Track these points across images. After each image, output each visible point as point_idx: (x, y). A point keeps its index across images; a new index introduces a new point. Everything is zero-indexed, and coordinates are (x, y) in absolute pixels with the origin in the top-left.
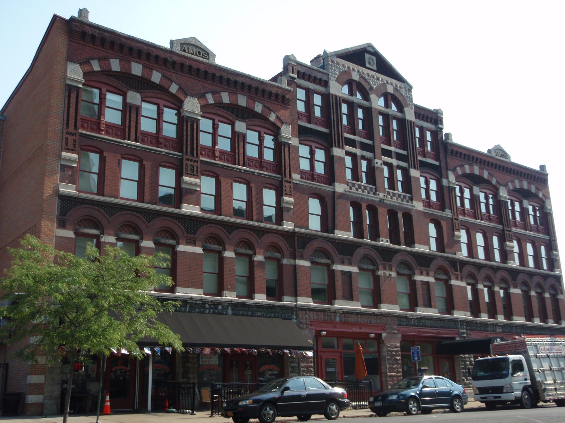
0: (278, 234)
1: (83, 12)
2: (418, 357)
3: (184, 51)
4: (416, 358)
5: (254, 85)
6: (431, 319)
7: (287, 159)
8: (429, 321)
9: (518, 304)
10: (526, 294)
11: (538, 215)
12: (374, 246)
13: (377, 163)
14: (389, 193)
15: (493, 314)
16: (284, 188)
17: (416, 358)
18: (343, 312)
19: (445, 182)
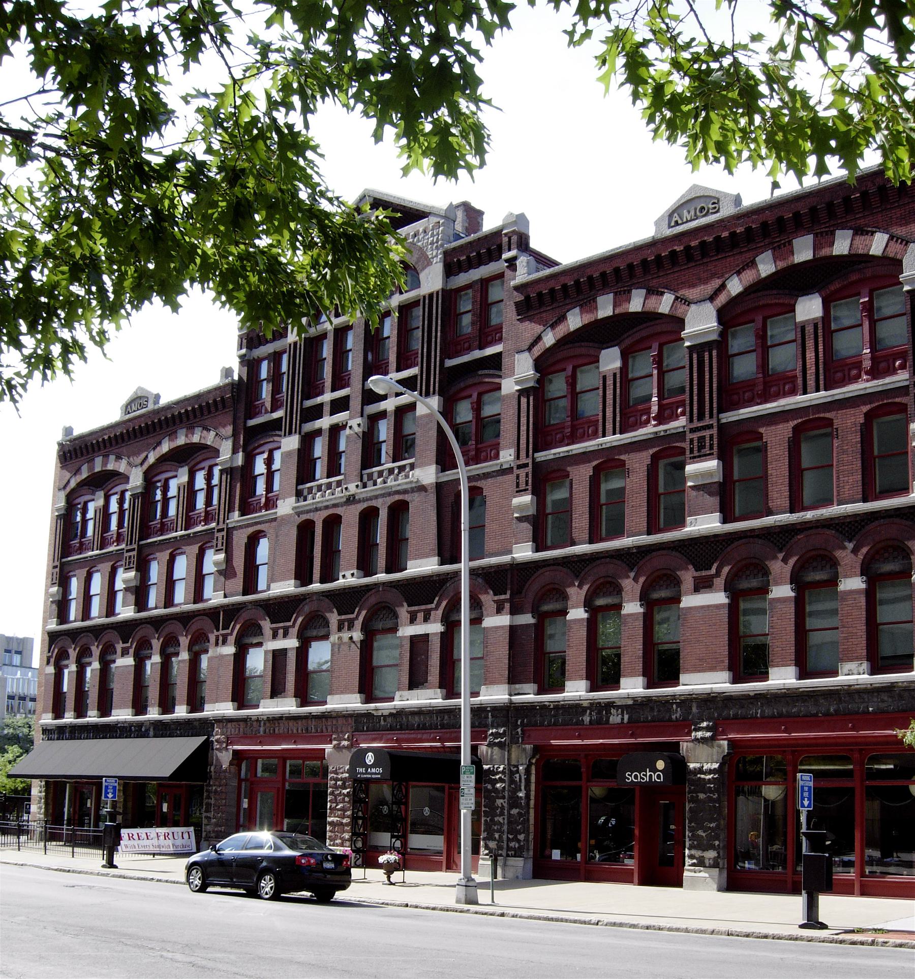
0: (559, 564)
1: (68, 431)
2: (114, 793)
3: (677, 224)
4: (110, 795)
5: (770, 217)
6: (419, 712)
7: (523, 420)
8: (417, 719)
9: (122, 688)
10: (139, 668)
11: (159, 492)
12: (391, 582)
13: (359, 425)
14: (339, 484)
15: (604, 673)
16: (530, 481)
17: (110, 795)
18: (268, 719)
19: (240, 460)
